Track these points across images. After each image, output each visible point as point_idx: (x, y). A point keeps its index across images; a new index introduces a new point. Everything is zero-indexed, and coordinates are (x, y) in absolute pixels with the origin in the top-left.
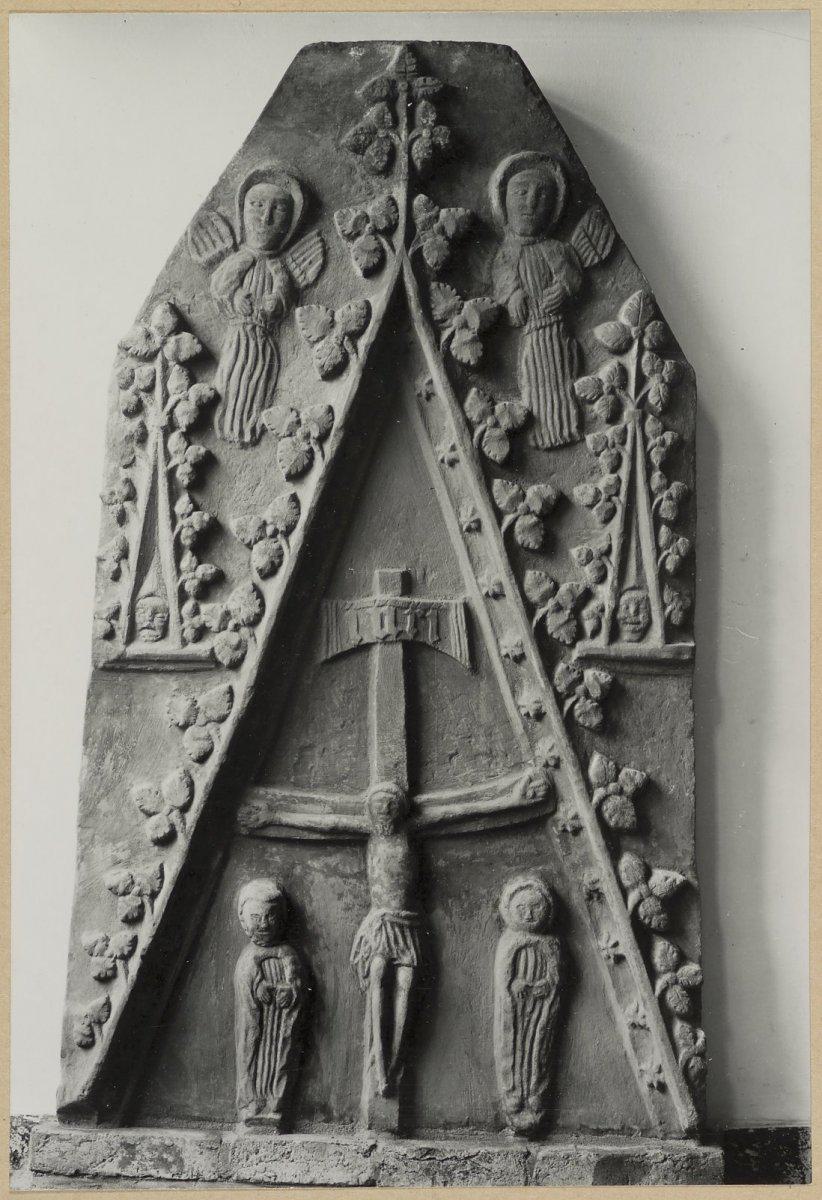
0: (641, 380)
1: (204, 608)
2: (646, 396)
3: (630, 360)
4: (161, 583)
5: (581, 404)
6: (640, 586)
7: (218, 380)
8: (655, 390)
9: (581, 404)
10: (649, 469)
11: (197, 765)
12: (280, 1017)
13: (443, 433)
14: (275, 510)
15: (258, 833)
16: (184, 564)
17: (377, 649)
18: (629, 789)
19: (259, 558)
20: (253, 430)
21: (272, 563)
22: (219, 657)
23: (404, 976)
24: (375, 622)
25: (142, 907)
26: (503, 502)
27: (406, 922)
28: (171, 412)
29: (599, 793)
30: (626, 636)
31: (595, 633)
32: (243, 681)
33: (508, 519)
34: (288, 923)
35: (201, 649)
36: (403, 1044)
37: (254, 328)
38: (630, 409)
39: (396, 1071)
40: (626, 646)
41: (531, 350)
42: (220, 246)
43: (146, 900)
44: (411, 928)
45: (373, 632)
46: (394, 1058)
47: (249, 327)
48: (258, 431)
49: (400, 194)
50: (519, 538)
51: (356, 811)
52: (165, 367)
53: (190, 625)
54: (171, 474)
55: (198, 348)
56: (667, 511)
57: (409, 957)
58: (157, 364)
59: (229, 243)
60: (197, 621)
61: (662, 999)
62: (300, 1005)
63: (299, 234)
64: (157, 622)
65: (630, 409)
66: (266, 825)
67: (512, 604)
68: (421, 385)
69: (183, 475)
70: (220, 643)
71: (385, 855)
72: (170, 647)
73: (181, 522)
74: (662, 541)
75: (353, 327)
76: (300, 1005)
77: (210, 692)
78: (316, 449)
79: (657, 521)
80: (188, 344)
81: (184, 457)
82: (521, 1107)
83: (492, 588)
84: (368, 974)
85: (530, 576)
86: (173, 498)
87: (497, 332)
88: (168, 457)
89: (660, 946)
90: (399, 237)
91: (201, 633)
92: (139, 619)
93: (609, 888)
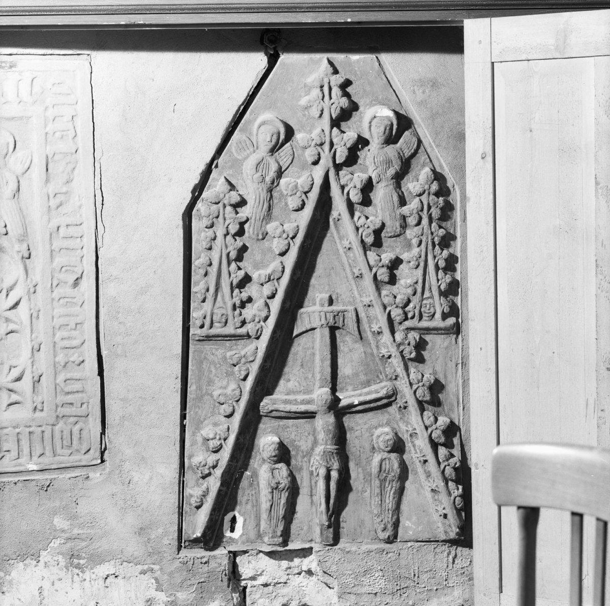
0: (429, 207)
1: (243, 311)
2: (431, 214)
3: (424, 198)
4: (225, 303)
5: (404, 218)
6: (432, 297)
7: (244, 212)
8: (436, 213)
9: (404, 218)
10: (434, 245)
11: (195, 509)
12: (281, 494)
13: (344, 232)
14: (274, 266)
15: (269, 415)
16: (234, 294)
17: (318, 331)
18: (427, 384)
19: (267, 290)
20: (263, 234)
21: (272, 293)
22: (250, 334)
23: (334, 475)
24: (317, 319)
25: (221, 444)
26: (372, 263)
27: (335, 451)
28: (227, 227)
29: (415, 387)
30: (424, 318)
31: (413, 318)
32: (263, 344)
33: (374, 270)
34: (283, 454)
35: (243, 331)
36: (334, 503)
37: (263, 189)
38: (425, 221)
39: (331, 516)
40: (425, 324)
41: (382, 194)
42: (248, 152)
43: (223, 442)
44: (336, 453)
45: (316, 323)
46: (331, 509)
47: (260, 189)
48: (265, 234)
49: (327, 128)
50: (379, 278)
51: (309, 402)
52: (225, 206)
53: (238, 320)
54: (228, 255)
55: (239, 199)
56: (442, 264)
57: (336, 465)
58: (221, 205)
59: (252, 149)
60: (242, 318)
61: (443, 472)
62: (289, 490)
63: (283, 145)
64: (224, 320)
65: (425, 221)
66: (272, 411)
67: (377, 311)
68: (334, 214)
69: (233, 255)
70: (250, 328)
71: (324, 423)
72: (230, 330)
73: (233, 275)
74: (440, 277)
75: (306, 190)
76: (289, 490)
77: (247, 348)
78: (291, 242)
79: (437, 268)
80: (234, 197)
81: (234, 246)
82: (384, 529)
83: (357, 273)
84: (318, 474)
85: (384, 293)
86: (229, 264)
87: (368, 187)
88: (226, 247)
89: (442, 451)
90: (326, 147)
91: (244, 323)
92: (214, 318)
93: (420, 429)
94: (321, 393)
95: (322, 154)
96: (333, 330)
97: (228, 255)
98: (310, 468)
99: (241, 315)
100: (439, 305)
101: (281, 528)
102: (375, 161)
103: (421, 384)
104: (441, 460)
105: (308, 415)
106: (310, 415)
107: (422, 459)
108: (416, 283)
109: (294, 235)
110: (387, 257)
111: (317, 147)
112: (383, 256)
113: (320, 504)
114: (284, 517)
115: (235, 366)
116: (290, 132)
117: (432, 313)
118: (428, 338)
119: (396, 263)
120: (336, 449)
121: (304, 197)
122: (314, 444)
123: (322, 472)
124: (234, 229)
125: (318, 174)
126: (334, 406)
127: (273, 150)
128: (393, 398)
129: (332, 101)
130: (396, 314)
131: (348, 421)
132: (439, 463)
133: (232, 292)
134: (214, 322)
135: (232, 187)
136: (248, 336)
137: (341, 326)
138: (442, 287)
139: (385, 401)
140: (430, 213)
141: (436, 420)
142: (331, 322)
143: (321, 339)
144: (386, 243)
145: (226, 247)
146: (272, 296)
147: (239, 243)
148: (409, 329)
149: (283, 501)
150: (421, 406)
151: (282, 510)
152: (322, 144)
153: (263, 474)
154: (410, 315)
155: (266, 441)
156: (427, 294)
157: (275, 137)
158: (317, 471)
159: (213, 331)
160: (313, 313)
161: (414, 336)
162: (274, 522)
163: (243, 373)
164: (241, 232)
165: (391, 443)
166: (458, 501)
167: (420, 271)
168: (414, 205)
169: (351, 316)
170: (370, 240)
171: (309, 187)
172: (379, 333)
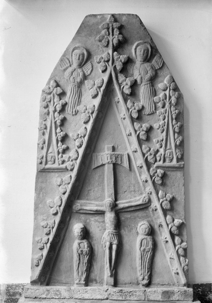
0: (170, 97)
1: (64, 156)
3: (167, 92)
4: (53, 150)
7: (66, 99)
8: (173, 100)
11: (63, 195)
13: (122, 110)
14: (81, 131)
16: (59, 145)
17: (106, 166)
19: (77, 143)
20: (75, 111)
22: (68, 168)
23: (114, 247)
26: (137, 129)
27: (115, 233)
31: (160, 160)
32: (74, 174)
34: (86, 234)
35: (63, 166)
37: (75, 86)
40: (167, 164)
41: (143, 90)
42: (67, 66)
43: (51, 229)
44: (116, 235)
45: (105, 161)
47: (74, 86)
48: (77, 112)
49: (110, 51)
51: (102, 206)
52: (54, 96)
54: (55, 122)
55: (62, 91)
56: (177, 130)
57: (115, 242)
58: (52, 95)
59: (69, 65)
60: (62, 159)
62: (89, 254)
64: (53, 160)
66: (80, 210)
67: (139, 153)
70: (68, 165)
71: (110, 217)
73: (58, 135)
74: (176, 137)
78: (91, 116)
79: (174, 132)
80: (59, 90)
82: (143, 279)
86: (56, 128)
87: (134, 85)
88: (55, 118)
89: (177, 239)
90: (110, 62)
91: (63, 162)
93: (164, 224)
94: (108, 199)
95: (99, 93)
96: (115, 166)
97: (55, 122)
98: (101, 243)
99: (62, 157)
100: (176, 154)
101: (84, 276)
102: (139, 71)
103: (164, 199)
104: (168, 223)
105: (100, 212)
106: (101, 213)
107: (165, 240)
108: (163, 140)
109: (92, 111)
110: (145, 126)
111: (105, 62)
112: (144, 125)
113: (107, 263)
114: (86, 270)
115: (52, 208)
116: (90, 56)
117: (171, 158)
118: (168, 173)
119: (150, 130)
120: (115, 233)
121: (98, 90)
122: (104, 233)
123: (108, 244)
124: (59, 108)
125: (106, 77)
126: (114, 207)
127: (81, 65)
128: (149, 205)
129: (114, 37)
130: (150, 159)
131: (124, 217)
132: (159, 199)
133: (57, 144)
134: (48, 161)
135: (58, 85)
136: (66, 169)
137: (119, 163)
138: (178, 143)
139: (144, 207)
140: (170, 101)
141: (173, 220)
142: (114, 162)
143: (108, 171)
144: (145, 118)
145: (55, 118)
146: (80, 146)
147: (62, 116)
148: (158, 167)
149: (86, 261)
150: (165, 212)
151: (85, 266)
152: (108, 61)
153: (75, 246)
154: (158, 159)
155: (76, 228)
156: (168, 147)
157: (81, 57)
158: (105, 244)
159: (48, 166)
160: (104, 156)
161: (160, 172)
162: (80, 274)
163: (64, 190)
164: (63, 110)
165: (147, 230)
166: (178, 240)
167: (165, 133)
168: (161, 95)
169: (125, 159)
170: (135, 115)
171: (60, 202)
172: (135, 152)
